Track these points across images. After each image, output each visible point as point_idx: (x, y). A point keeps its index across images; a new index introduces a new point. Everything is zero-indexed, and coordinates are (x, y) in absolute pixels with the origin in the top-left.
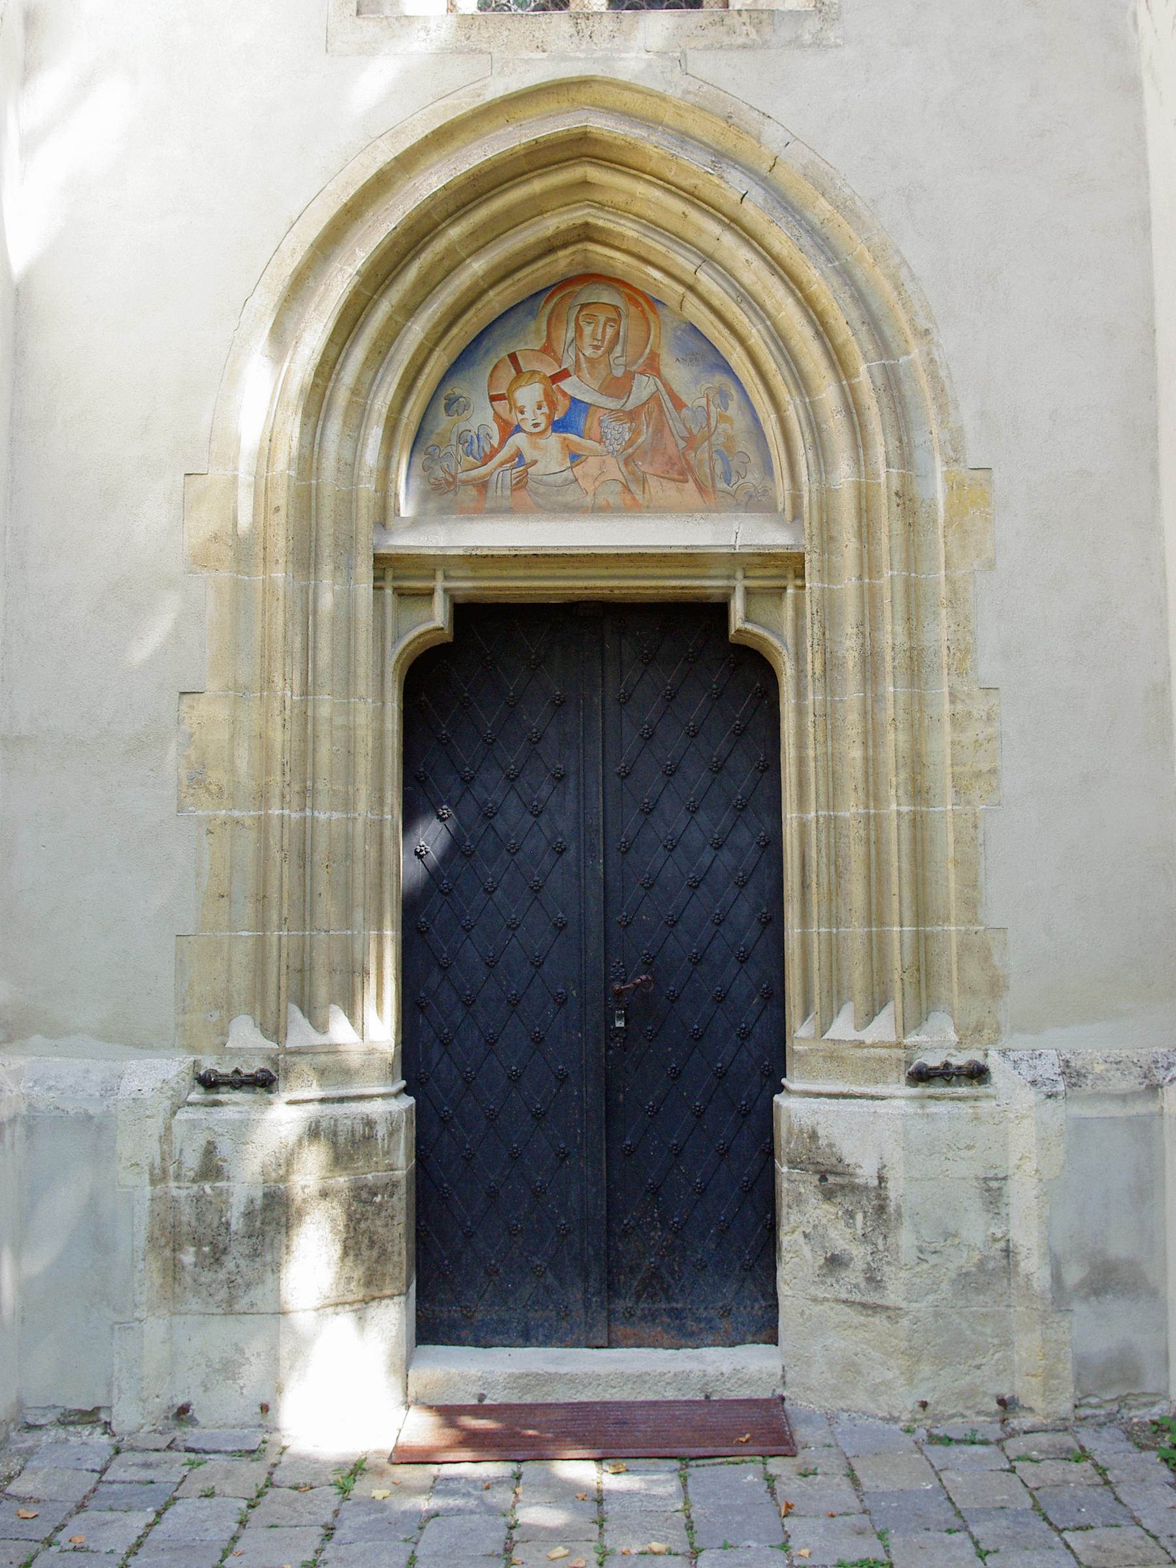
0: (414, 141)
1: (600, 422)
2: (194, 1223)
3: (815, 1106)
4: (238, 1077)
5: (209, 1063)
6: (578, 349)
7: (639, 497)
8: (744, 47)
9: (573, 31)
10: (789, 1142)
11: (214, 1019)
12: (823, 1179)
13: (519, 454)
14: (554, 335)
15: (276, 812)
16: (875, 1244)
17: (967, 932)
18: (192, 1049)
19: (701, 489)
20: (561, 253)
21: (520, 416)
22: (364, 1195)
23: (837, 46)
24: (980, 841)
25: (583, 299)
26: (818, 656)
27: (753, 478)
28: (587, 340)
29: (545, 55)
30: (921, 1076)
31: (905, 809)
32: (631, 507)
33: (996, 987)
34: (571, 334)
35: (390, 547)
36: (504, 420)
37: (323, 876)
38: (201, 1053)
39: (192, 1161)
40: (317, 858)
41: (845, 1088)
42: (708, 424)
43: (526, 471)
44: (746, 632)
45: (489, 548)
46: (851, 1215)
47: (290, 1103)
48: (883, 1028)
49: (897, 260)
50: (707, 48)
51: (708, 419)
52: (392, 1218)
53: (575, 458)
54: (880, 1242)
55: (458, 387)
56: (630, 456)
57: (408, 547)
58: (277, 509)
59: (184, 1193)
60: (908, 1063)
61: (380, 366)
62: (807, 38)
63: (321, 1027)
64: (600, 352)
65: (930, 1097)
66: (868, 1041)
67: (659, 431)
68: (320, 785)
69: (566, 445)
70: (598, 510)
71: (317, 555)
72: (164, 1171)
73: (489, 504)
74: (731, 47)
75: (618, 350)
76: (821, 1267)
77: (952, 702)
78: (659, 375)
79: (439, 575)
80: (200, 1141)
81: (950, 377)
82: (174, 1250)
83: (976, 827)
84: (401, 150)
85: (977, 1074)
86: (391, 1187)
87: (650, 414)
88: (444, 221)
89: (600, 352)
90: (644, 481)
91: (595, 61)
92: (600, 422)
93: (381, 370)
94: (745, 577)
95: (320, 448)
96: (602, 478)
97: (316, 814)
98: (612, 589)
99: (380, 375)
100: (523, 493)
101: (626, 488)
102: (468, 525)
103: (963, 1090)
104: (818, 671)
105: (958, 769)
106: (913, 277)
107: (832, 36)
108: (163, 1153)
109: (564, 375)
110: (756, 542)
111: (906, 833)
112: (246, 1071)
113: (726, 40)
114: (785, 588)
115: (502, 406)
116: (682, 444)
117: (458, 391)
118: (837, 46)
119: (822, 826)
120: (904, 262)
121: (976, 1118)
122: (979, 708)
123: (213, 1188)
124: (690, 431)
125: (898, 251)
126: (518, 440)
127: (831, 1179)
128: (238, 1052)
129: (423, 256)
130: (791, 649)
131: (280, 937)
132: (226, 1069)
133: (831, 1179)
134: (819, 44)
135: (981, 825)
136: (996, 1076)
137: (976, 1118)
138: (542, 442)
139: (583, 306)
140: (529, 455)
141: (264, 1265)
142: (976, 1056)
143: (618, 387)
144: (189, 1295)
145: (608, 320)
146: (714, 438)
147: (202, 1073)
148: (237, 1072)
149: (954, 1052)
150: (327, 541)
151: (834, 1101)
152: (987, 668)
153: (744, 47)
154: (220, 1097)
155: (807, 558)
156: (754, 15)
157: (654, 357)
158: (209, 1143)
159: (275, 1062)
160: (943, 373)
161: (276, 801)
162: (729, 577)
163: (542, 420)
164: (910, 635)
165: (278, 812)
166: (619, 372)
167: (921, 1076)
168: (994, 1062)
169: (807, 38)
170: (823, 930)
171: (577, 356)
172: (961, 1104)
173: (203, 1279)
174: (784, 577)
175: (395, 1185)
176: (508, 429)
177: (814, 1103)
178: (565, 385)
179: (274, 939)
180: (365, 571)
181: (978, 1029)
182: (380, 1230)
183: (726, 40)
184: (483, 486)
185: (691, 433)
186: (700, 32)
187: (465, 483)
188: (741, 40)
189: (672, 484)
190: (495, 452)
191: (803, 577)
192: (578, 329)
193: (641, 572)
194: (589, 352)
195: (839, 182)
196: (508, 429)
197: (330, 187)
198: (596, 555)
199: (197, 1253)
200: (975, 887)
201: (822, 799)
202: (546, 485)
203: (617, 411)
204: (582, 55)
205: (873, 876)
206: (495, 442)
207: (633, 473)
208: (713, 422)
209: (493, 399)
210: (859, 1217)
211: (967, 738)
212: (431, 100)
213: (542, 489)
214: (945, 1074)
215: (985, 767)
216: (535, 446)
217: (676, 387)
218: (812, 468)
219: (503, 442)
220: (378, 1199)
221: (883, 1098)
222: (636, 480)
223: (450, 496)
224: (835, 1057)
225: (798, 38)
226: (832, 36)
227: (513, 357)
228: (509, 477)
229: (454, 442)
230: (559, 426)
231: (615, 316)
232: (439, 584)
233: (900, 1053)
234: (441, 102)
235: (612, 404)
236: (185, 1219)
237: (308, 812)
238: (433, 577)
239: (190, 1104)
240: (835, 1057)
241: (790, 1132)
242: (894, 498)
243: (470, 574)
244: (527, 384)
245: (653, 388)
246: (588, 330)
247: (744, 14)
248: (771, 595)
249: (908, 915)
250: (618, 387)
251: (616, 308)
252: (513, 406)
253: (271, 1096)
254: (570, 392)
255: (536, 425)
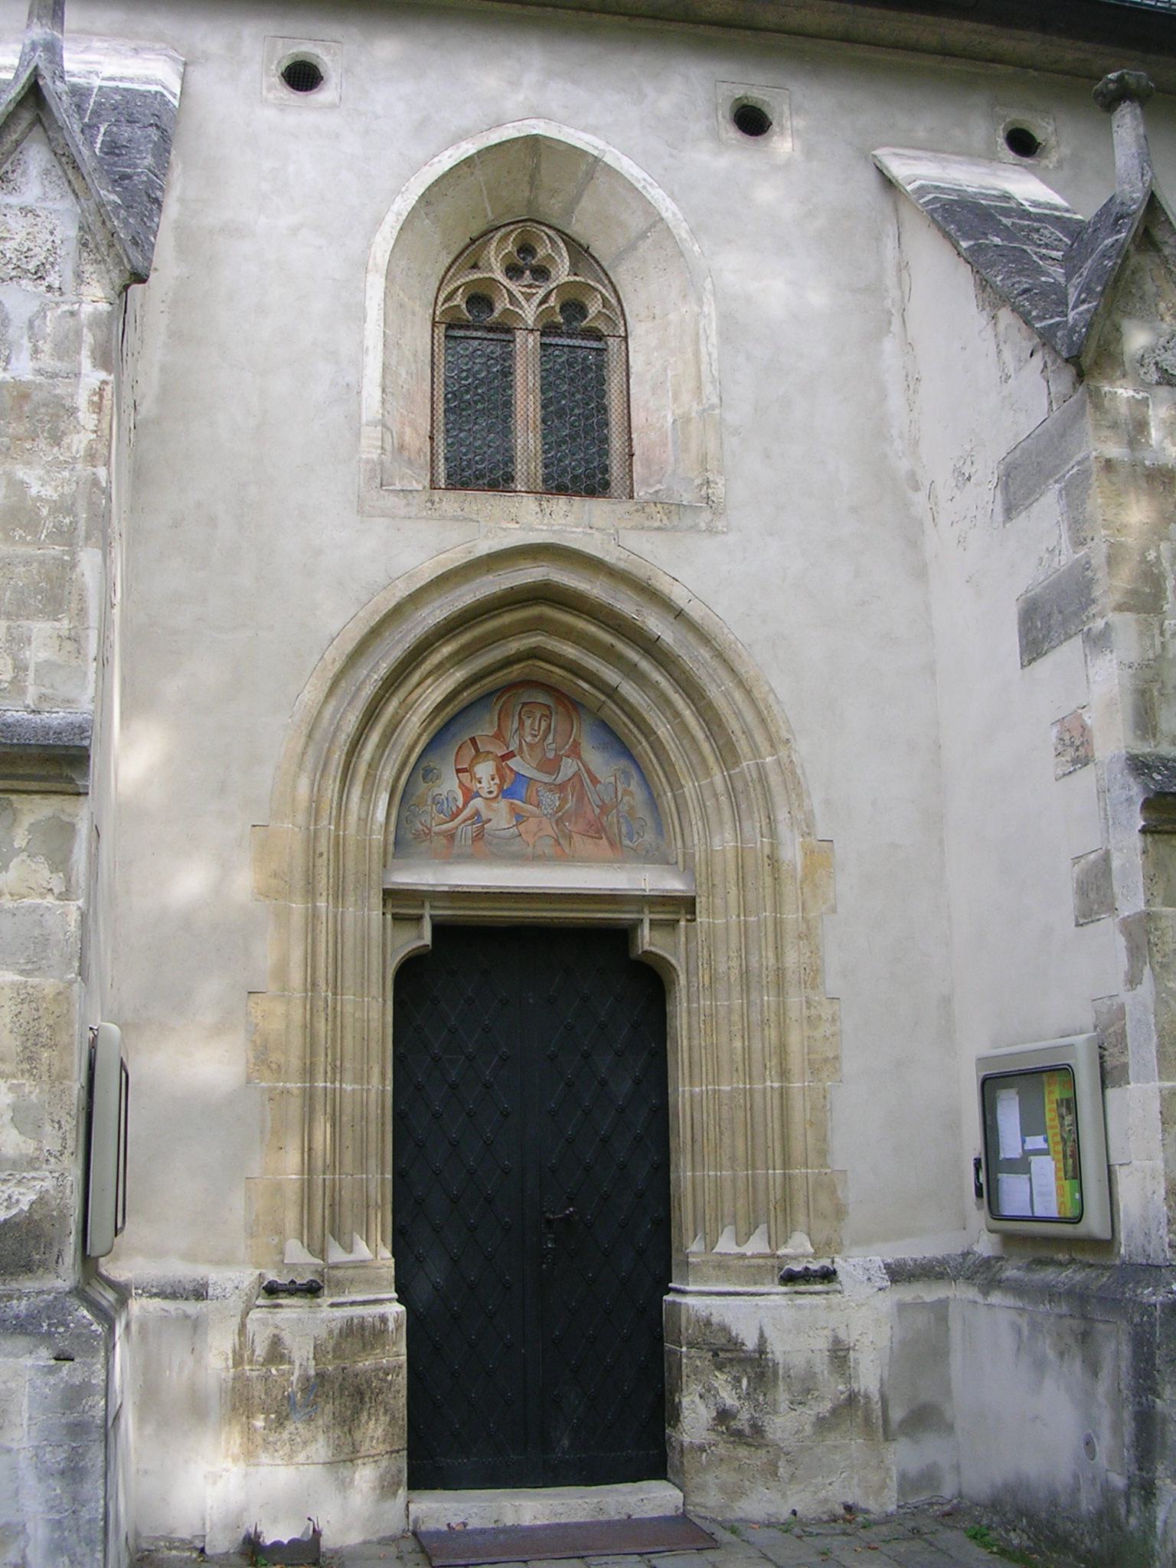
0: (423, 583)
1: (537, 791)
2: (263, 1397)
3: (709, 1302)
4: (292, 1286)
5: (271, 1276)
6: (521, 737)
7: (567, 850)
8: (659, 529)
9: (538, 509)
10: (687, 1330)
11: (274, 1243)
12: (716, 1355)
13: (477, 813)
14: (503, 725)
15: (768, 1083)
16: (757, 1400)
17: (820, 1173)
18: (257, 1265)
19: (612, 844)
20: (516, 667)
21: (479, 785)
22: (381, 1375)
23: (723, 533)
24: (828, 1107)
25: (525, 699)
26: (707, 972)
27: (649, 837)
28: (527, 730)
29: (517, 526)
30: (789, 1278)
31: (776, 1085)
32: (561, 857)
33: (840, 1212)
34: (516, 725)
35: (394, 883)
36: (466, 788)
37: (348, 1132)
38: (266, 1268)
39: (261, 1351)
40: (345, 1119)
41: (731, 1289)
42: (616, 796)
43: (483, 826)
44: (651, 952)
45: (467, 886)
46: (738, 1380)
47: (332, 1305)
48: (757, 1245)
49: (767, 689)
50: (632, 528)
51: (616, 793)
52: (398, 1392)
53: (519, 818)
54: (761, 1398)
55: (432, 761)
56: (560, 817)
57: (407, 884)
58: (321, 855)
59: (256, 1373)
60: (780, 1269)
61: (386, 746)
62: (703, 525)
63: (349, 1248)
64: (537, 739)
65: (797, 1293)
66: (749, 1253)
67: (581, 799)
68: (347, 1065)
69: (513, 809)
70: (536, 859)
71: (344, 889)
72: (241, 1357)
73: (455, 851)
74: (650, 529)
75: (551, 737)
76: (714, 1419)
77: (808, 1008)
78: (580, 758)
79: (427, 905)
80: (270, 1331)
81: (804, 774)
82: (248, 1417)
83: (825, 1097)
84: (414, 589)
85: (828, 1275)
86: (395, 1369)
87: (574, 787)
88: (438, 640)
89: (537, 739)
90: (571, 837)
91: (555, 532)
92: (537, 791)
93: (388, 750)
94: (650, 912)
95: (346, 807)
96: (541, 834)
97: (344, 1086)
98: (551, 918)
99: (386, 753)
100: (481, 843)
101: (557, 841)
102: (448, 868)
103: (818, 1287)
104: (707, 984)
105: (812, 1056)
106: (778, 702)
107: (720, 525)
108: (241, 1343)
109: (510, 755)
110: (661, 887)
111: (776, 1101)
112: (299, 1281)
113: (647, 524)
114: (678, 921)
115: (465, 776)
116: (597, 811)
117: (432, 765)
118: (723, 533)
119: (711, 1097)
120: (771, 690)
121: (829, 1307)
122: (826, 1012)
123: (277, 1370)
124: (602, 801)
125: (767, 682)
126: (478, 802)
127: (722, 1355)
128: (292, 1267)
129: (423, 667)
130: (684, 964)
131: (324, 1179)
132: (283, 1280)
133: (722, 1355)
134: (711, 531)
135: (828, 1096)
136: (841, 1275)
137: (829, 1307)
138: (495, 805)
139: (524, 704)
140: (485, 814)
141: (317, 1427)
142: (826, 1262)
143: (550, 766)
144: (260, 1451)
145: (543, 715)
146: (620, 807)
147: (265, 1283)
148: (293, 1282)
149: (811, 1259)
150: (351, 879)
151: (722, 1298)
152: (832, 983)
153: (659, 529)
154: (280, 1301)
155: (698, 900)
156: (666, 506)
157: (576, 745)
158: (274, 1335)
159: (322, 1275)
160: (799, 771)
161: (320, 1075)
162: (638, 912)
163: (495, 789)
164: (777, 960)
165: (322, 1085)
166: (551, 755)
167: (789, 1278)
168: (840, 1264)
169: (703, 525)
170: (712, 1173)
171: (520, 741)
172: (817, 1297)
173: (271, 1439)
174: (678, 913)
175: (400, 1367)
176: (469, 795)
177: (708, 1300)
178: (511, 763)
179: (320, 1181)
180: (376, 899)
181: (828, 1243)
182: (391, 1402)
183: (647, 524)
184: (451, 836)
185: (603, 802)
186: (627, 516)
187: (438, 834)
188: (657, 524)
189: (590, 840)
190: (460, 811)
191: (694, 913)
192: (521, 722)
193: (575, 906)
194: (529, 739)
195: (726, 630)
196: (469, 795)
197: (361, 614)
198: (545, 894)
199: (265, 1419)
200: (825, 1140)
201: (710, 1076)
202: (499, 837)
203: (550, 784)
204: (545, 528)
205: (749, 1133)
206: (460, 804)
207: (562, 831)
208: (620, 796)
209: (458, 771)
210: (745, 1382)
211: (818, 1034)
212: (435, 553)
213: (495, 841)
214: (806, 1276)
215: (831, 1055)
216: (489, 807)
217: (592, 768)
218: (701, 834)
219: (465, 804)
220: (389, 1378)
221: (763, 1294)
222: (564, 836)
223: (427, 843)
224: (723, 1266)
225: (696, 525)
226: (720, 525)
227: (473, 740)
228: (470, 830)
229: (429, 802)
230: (505, 793)
231: (548, 713)
232: (427, 912)
233: (775, 1262)
234: (442, 556)
235: (546, 779)
236: (256, 1394)
237: (338, 1085)
238: (422, 906)
239: (258, 1307)
240: (723, 1266)
241: (688, 1319)
242: (766, 859)
243: (450, 905)
244: (484, 761)
245: (575, 768)
246: (528, 722)
247: (659, 505)
248: (667, 925)
249: (778, 1162)
250: (550, 766)
251: (548, 707)
252: (473, 776)
253: (319, 1300)
254: (515, 769)
255: (491, 792)
